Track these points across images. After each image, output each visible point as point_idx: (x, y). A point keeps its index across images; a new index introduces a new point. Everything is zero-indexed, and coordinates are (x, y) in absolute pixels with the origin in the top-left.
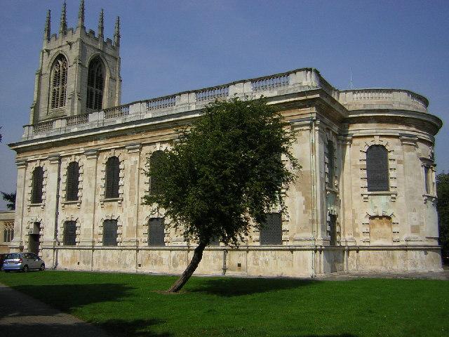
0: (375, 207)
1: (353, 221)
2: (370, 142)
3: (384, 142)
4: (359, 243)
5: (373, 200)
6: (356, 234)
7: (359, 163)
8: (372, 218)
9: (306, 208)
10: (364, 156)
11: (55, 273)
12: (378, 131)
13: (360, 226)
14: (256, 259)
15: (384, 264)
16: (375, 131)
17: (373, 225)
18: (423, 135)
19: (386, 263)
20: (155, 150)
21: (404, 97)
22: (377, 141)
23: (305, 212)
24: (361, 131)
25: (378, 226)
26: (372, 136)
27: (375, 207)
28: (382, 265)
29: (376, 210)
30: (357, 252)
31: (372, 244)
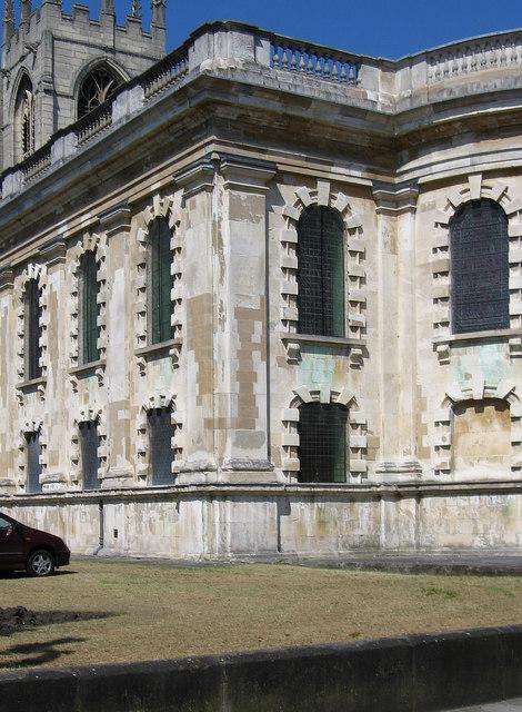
0: (468, 376)
1: (418, 418)
2: (456, 195)
3: (340, 201)
4: (428, 475)
5: (463, 358)
6: (423, 453)
7: (433, 258)
8: (459, 407)
9: (202, 391)
10: (443, 236)
11: (388, 551)
12: (477, 159)
13: (431, 428)
14: (139, 519)
15: (480, 527)
16: (467, 161)
17: (466, 427)
18: (88, 216)
19: (486, 530)
20: (466, 198)
21: (118, 106)
22: (475, 189)
23: (199, 401)
24: (435, 168)
25: (476, 426)
26: (463, 179)
27: (468, 376)
28: (476, 533)
29: (468, 385)
30: (418, 501)
31: (458, 476)
